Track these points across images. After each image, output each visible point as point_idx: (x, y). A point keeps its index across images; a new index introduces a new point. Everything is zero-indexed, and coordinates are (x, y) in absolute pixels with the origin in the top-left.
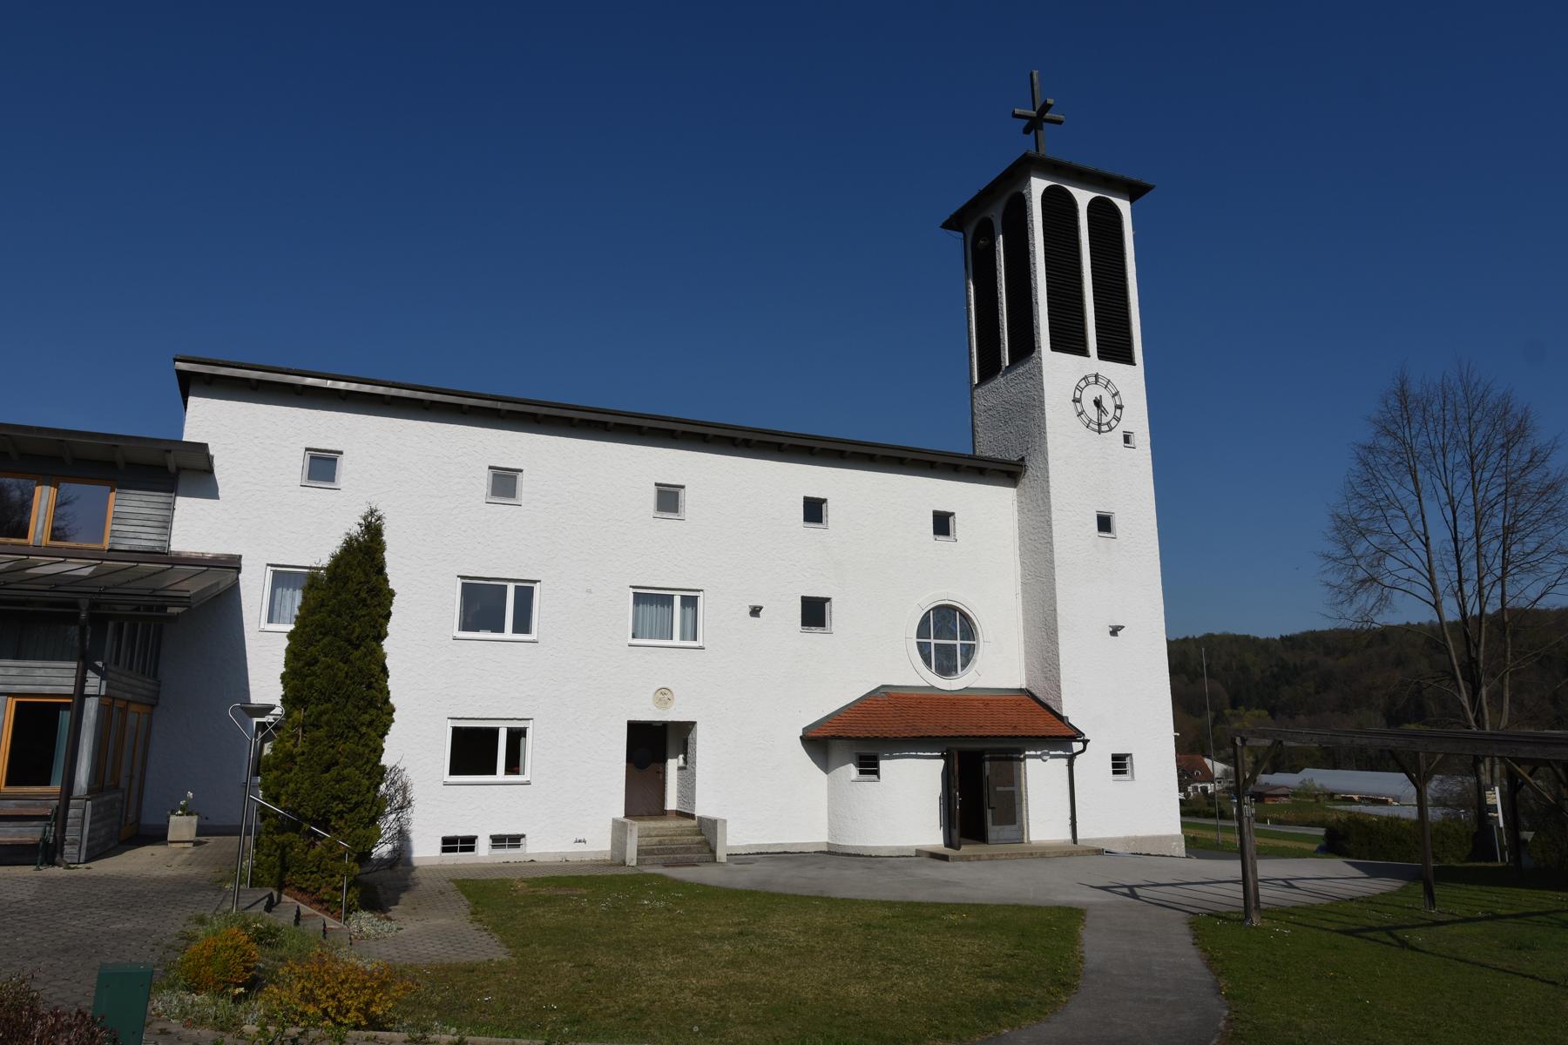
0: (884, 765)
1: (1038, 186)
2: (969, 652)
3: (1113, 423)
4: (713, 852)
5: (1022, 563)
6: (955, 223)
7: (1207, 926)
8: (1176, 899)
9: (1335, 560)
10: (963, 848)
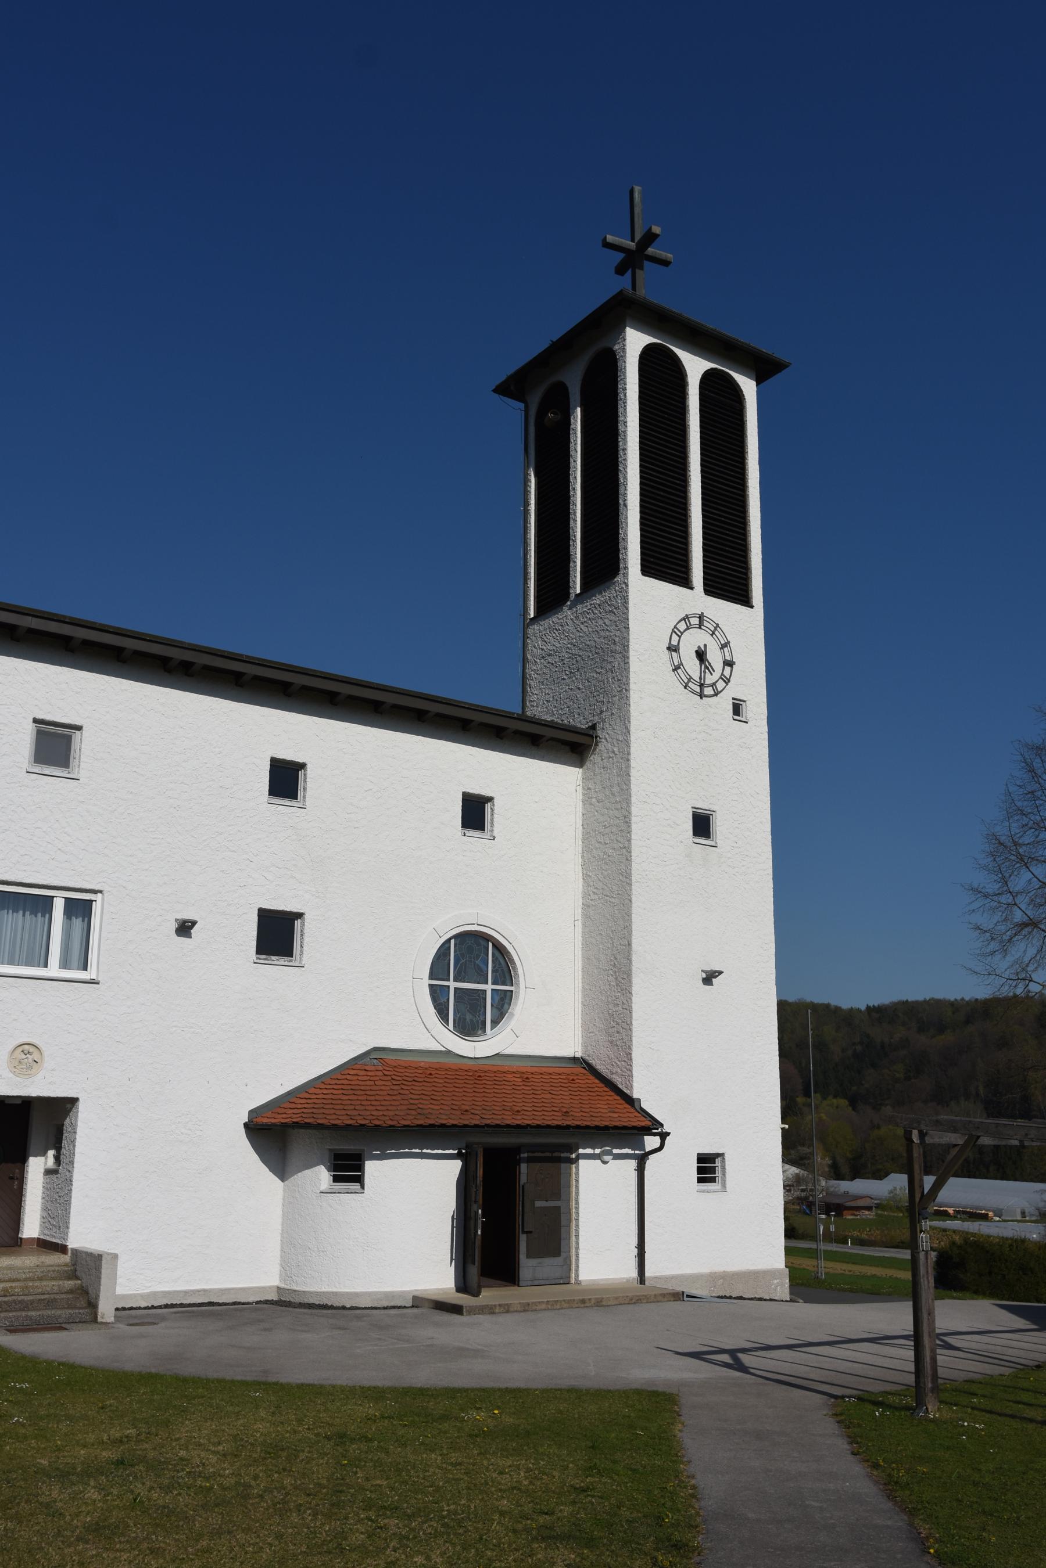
0: (371, 1167)
1: (635, 341)
2: (504, 1002)
3: (720, 685)
4: (93, 1306)
5: (586, 877)
6: (513, 387)
7: (865, 1415)
8: (802, 1371)
9: (986, 896)
10: (485, 1293)
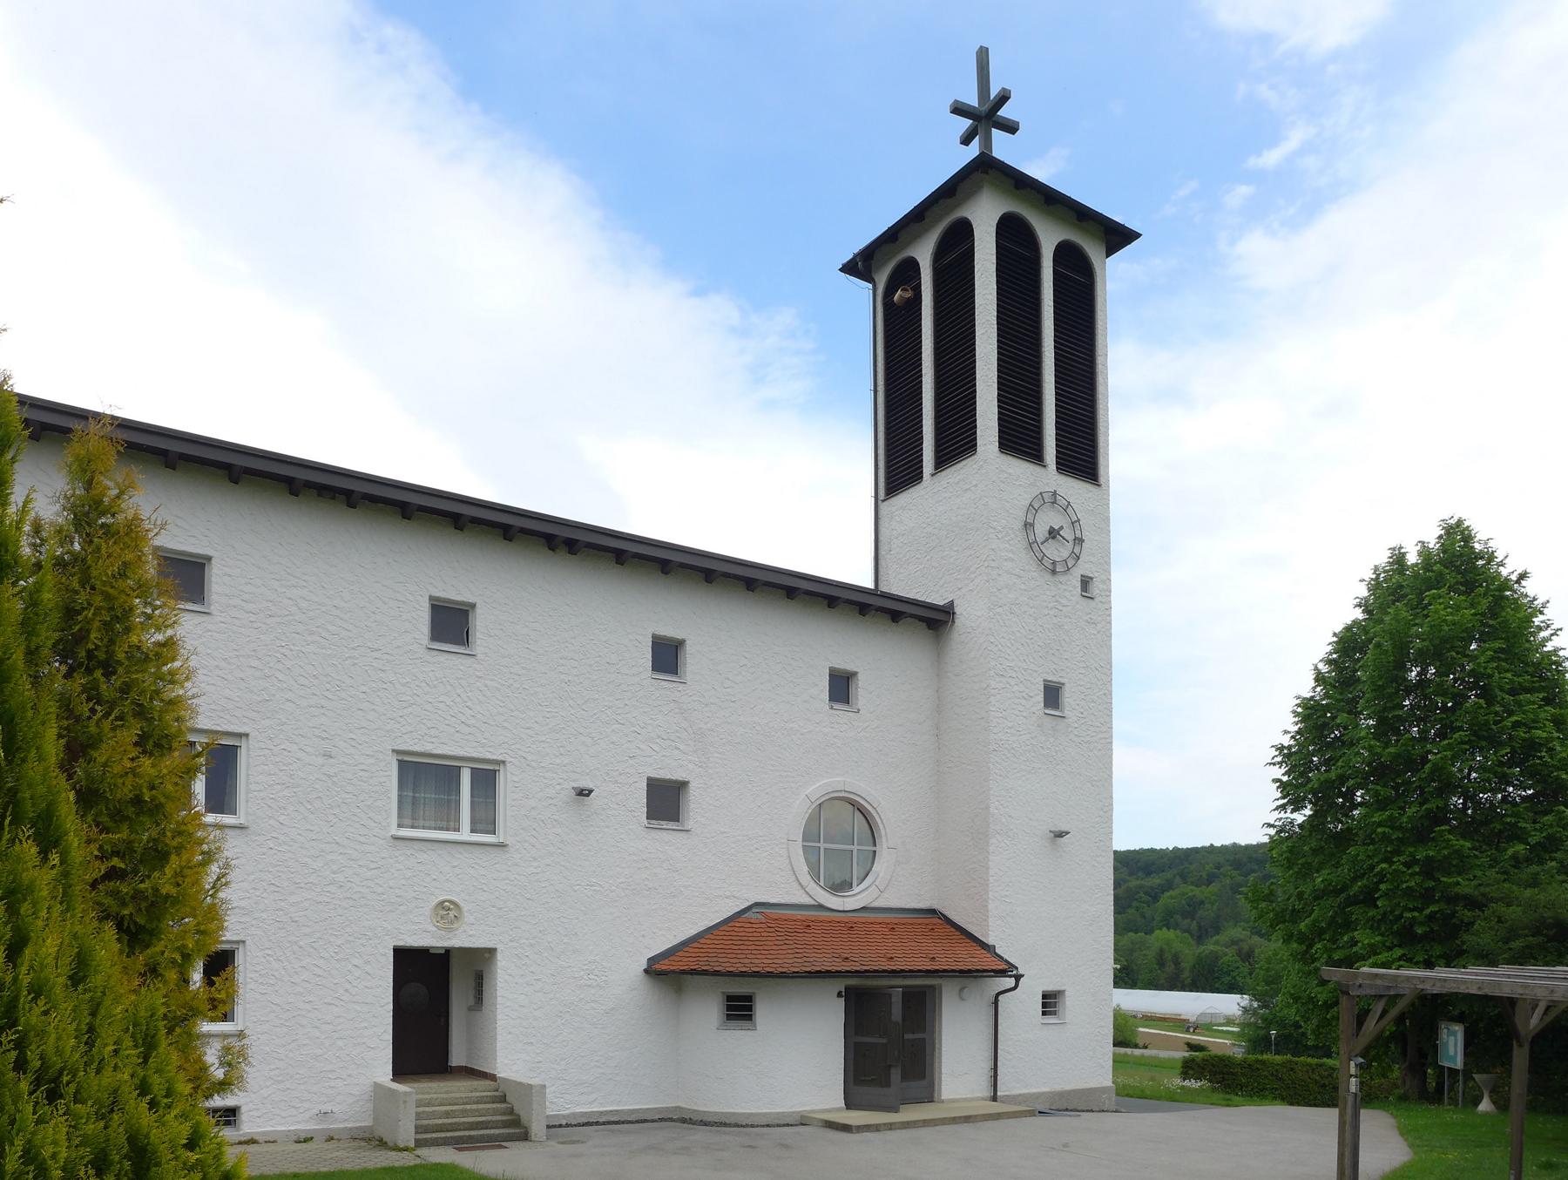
6: (860, 266)
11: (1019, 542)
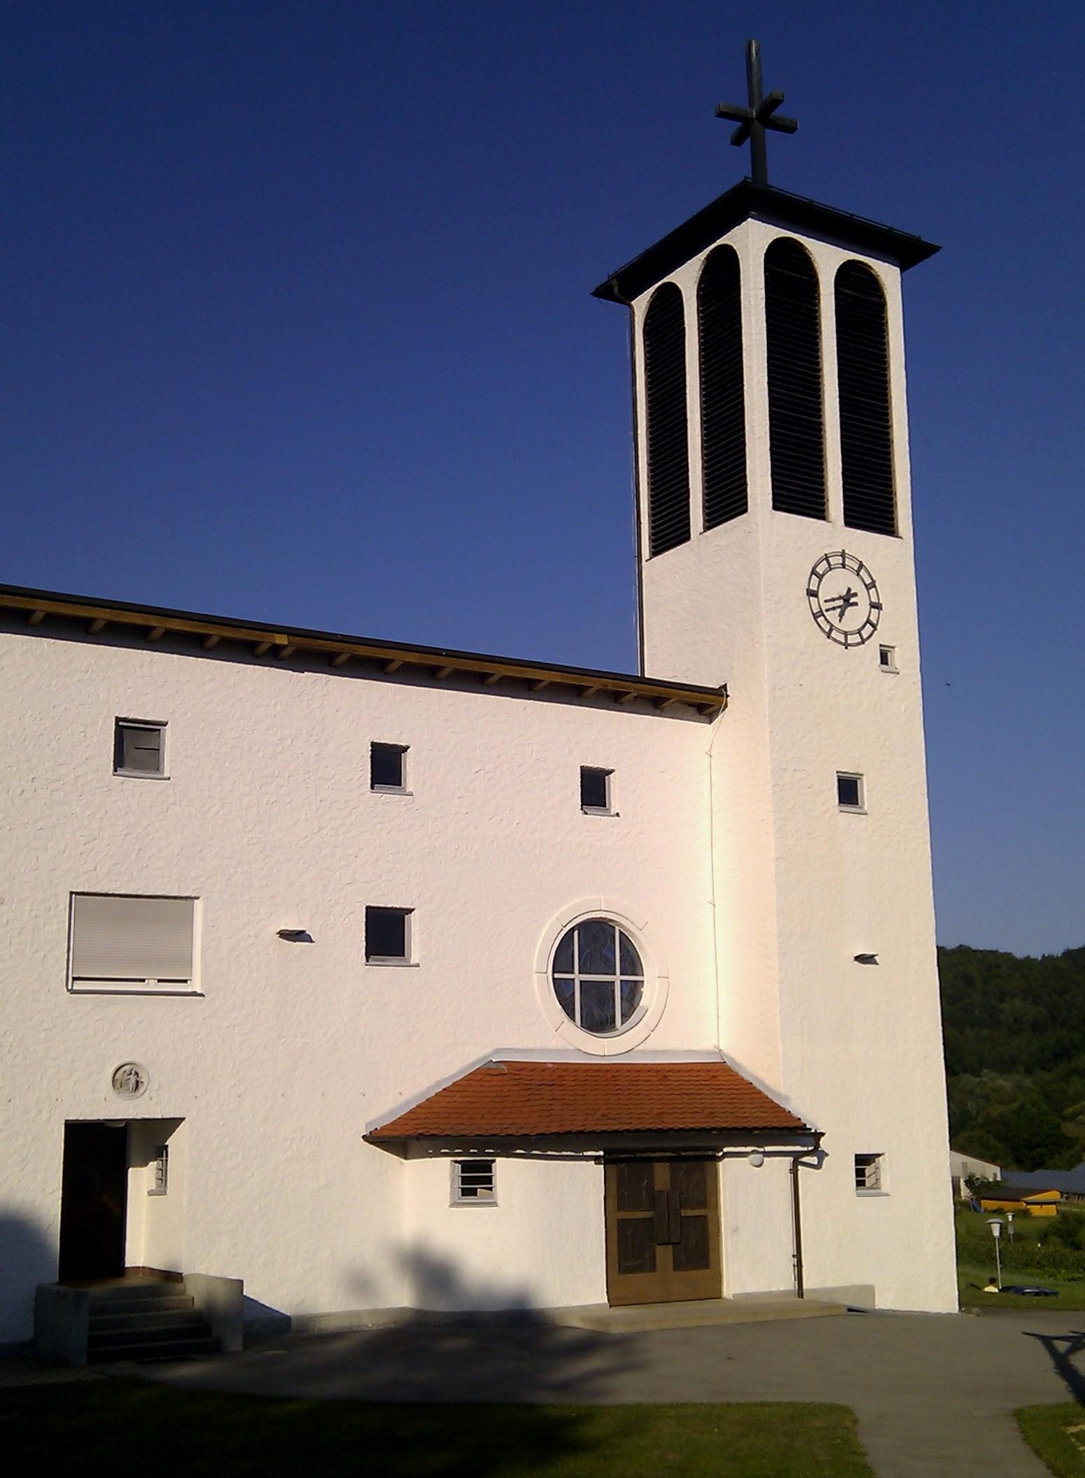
11: (803, 608)
